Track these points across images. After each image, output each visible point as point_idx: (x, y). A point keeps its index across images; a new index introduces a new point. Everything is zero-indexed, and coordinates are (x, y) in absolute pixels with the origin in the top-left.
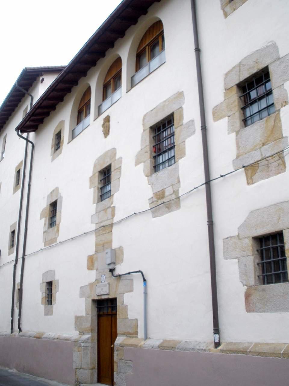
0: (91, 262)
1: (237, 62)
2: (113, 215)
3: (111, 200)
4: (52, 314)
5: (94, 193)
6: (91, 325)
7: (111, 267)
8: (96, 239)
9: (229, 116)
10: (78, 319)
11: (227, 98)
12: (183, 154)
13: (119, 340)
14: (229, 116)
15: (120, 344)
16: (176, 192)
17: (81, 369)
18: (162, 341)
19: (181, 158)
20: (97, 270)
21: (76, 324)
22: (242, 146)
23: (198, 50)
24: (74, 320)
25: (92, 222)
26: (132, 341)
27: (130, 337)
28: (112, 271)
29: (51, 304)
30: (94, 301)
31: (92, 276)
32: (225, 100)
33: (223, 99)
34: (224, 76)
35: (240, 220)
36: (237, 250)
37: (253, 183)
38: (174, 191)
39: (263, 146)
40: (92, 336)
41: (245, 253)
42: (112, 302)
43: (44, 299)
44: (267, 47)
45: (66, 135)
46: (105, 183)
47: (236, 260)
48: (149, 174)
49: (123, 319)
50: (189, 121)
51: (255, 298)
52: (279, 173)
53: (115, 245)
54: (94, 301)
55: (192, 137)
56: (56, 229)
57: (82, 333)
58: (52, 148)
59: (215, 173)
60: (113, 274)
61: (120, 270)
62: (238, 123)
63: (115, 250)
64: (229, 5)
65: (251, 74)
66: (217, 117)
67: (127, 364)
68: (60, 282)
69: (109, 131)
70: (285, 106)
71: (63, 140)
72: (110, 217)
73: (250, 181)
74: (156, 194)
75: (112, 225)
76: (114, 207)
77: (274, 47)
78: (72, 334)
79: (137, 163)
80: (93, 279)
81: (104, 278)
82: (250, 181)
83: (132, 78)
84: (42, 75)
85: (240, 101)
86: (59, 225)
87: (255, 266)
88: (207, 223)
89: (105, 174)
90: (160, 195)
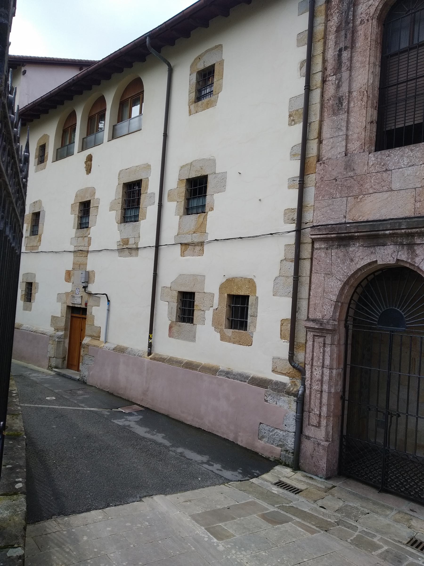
0: (69, 276)
1: (189, 161)
2: (89, 244)
3: (89, 231)
4: (30, 310)
5: (75, 219)
6: (65, 325)
7: (84, 285)
8: (74, 259)
9: (178, 202)
10: (54, 318)
11: (179, 187)
12: (144, 218)
13: (86, 340)
14: (178, 202)
15: (86, 344)
16: (136, 243)
17: (54, 358)
18: (116, 346)
19: (143, 219)
20: (73, 283)
21: (52, 322)
22: (182, 228)
23: (165, 135)
24: (51, 318)
25: (71, 244)
26: (95, 342)
27: (94, 339)
28: (85, 288)
29: (30, 301)
30: (68, 307)
31: (68, 287)
32: (177, 188)
33: (176, 187)
34: (180, 168)
35: (173, 278)
36: (169, 296)
37: (184, 256)
38: (135, 243)
39: (194, 233)
40: (65, 334)
41: (173, 300)
42: (84, 311)
43: (24, 296)
44: (210, 159)
45: (50, 151)
46: (84, 214)
47: (167, 303)
48: (119, 222)
49: (90, 325)
50: (152, 193)
51: (175, 329)
52: (200, 256)
53: (89, 268)
54: (68, 307)
55: (152, 206)
56: (38, 238)
57: (57, 330)
58: (35, 158)
59: (163, 242)
60: (85, 290)
61: (92, 288)
62: (182, 210)
63: (88, 272)
64: (193, 105)
65: (196, 176)
66: (170, 200)
67: (90, 358)
68: (39, 285)
69: (90, 170)
70: (211, 211)
71: (47, 156)
72: (87, 245)
73: (183, 254)
74: (122, 240)
75: (88, 252)
76: (91, 238)
77: (212, 162)
78: (49, 329)
79: (111, 209)
80: (69, 290)
81: (78, 291)
82: (183, 254)
83: (114, 126)
84: (23, 66)
85: (187, 193)
86: (41, 235)
87: (177, 310)
88: (153, 274)
89: (85, 207)
90: (125, 242)
